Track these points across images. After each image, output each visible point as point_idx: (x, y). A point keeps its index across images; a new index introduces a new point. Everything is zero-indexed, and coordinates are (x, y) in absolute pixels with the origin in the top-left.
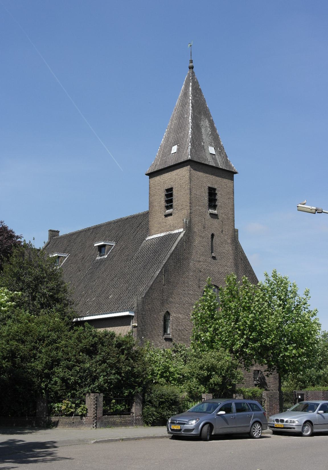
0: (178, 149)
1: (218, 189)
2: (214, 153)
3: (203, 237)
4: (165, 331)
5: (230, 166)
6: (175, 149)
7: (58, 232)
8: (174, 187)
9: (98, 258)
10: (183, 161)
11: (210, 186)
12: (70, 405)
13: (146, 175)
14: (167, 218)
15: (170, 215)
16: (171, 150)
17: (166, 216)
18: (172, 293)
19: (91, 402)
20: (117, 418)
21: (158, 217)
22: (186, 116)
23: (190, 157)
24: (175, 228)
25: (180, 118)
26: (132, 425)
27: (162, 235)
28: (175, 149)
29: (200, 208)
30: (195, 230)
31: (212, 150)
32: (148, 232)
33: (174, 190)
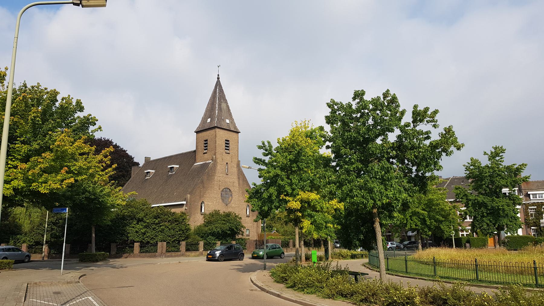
4: (201, 211)
6: (209, 120)
12: (429, 119)
19: (162, 246)
20: (173, 254)
21: (199, 155)
24: (208, 160)
28: (209, 120)
31: (228, 121)
32: (195, 161)
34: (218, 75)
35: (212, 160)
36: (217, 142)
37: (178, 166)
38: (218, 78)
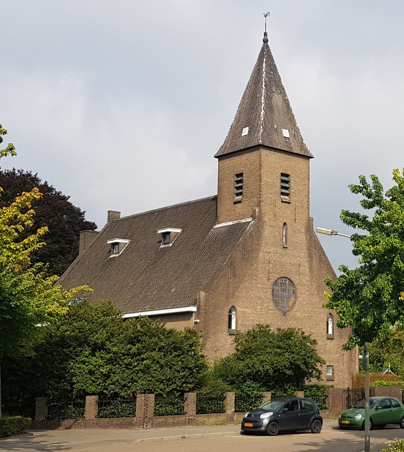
0: (249, 132)
1: (291, 175)
2: (289, 137)
3: (274, 227)
4: (230, 326)
5: (306, 150)
6: (245, 131)
7: (120, 213)
8: (244, 173)
9: (162, 246)
10: (253, 145)
11: (283, 172)
13: (215, 157)
14: (236, 205)
15: (240, 202)
16: (242, 132)
17: (235, 203)
18: (238, 287)
19: (145, 403)
20: (170, 419)
22: (258, 96)
23: (260, 141)
24: (245, 217)
25: (252, 97)
26: (185, 425)
27: (231, 223)
28: (245, 131)
29: (271, 196)
30: (266, 219)
31: (286, 133)
32: (216, 220)
33: (244, 175)
34: (265, 34)
35: (253, 217)
36: (264, 179)
37: (179, 231)
38: (265, 41)
